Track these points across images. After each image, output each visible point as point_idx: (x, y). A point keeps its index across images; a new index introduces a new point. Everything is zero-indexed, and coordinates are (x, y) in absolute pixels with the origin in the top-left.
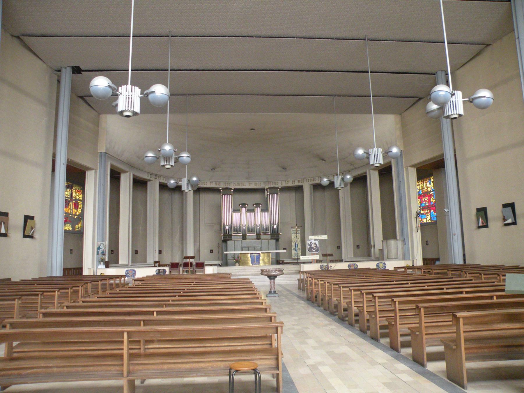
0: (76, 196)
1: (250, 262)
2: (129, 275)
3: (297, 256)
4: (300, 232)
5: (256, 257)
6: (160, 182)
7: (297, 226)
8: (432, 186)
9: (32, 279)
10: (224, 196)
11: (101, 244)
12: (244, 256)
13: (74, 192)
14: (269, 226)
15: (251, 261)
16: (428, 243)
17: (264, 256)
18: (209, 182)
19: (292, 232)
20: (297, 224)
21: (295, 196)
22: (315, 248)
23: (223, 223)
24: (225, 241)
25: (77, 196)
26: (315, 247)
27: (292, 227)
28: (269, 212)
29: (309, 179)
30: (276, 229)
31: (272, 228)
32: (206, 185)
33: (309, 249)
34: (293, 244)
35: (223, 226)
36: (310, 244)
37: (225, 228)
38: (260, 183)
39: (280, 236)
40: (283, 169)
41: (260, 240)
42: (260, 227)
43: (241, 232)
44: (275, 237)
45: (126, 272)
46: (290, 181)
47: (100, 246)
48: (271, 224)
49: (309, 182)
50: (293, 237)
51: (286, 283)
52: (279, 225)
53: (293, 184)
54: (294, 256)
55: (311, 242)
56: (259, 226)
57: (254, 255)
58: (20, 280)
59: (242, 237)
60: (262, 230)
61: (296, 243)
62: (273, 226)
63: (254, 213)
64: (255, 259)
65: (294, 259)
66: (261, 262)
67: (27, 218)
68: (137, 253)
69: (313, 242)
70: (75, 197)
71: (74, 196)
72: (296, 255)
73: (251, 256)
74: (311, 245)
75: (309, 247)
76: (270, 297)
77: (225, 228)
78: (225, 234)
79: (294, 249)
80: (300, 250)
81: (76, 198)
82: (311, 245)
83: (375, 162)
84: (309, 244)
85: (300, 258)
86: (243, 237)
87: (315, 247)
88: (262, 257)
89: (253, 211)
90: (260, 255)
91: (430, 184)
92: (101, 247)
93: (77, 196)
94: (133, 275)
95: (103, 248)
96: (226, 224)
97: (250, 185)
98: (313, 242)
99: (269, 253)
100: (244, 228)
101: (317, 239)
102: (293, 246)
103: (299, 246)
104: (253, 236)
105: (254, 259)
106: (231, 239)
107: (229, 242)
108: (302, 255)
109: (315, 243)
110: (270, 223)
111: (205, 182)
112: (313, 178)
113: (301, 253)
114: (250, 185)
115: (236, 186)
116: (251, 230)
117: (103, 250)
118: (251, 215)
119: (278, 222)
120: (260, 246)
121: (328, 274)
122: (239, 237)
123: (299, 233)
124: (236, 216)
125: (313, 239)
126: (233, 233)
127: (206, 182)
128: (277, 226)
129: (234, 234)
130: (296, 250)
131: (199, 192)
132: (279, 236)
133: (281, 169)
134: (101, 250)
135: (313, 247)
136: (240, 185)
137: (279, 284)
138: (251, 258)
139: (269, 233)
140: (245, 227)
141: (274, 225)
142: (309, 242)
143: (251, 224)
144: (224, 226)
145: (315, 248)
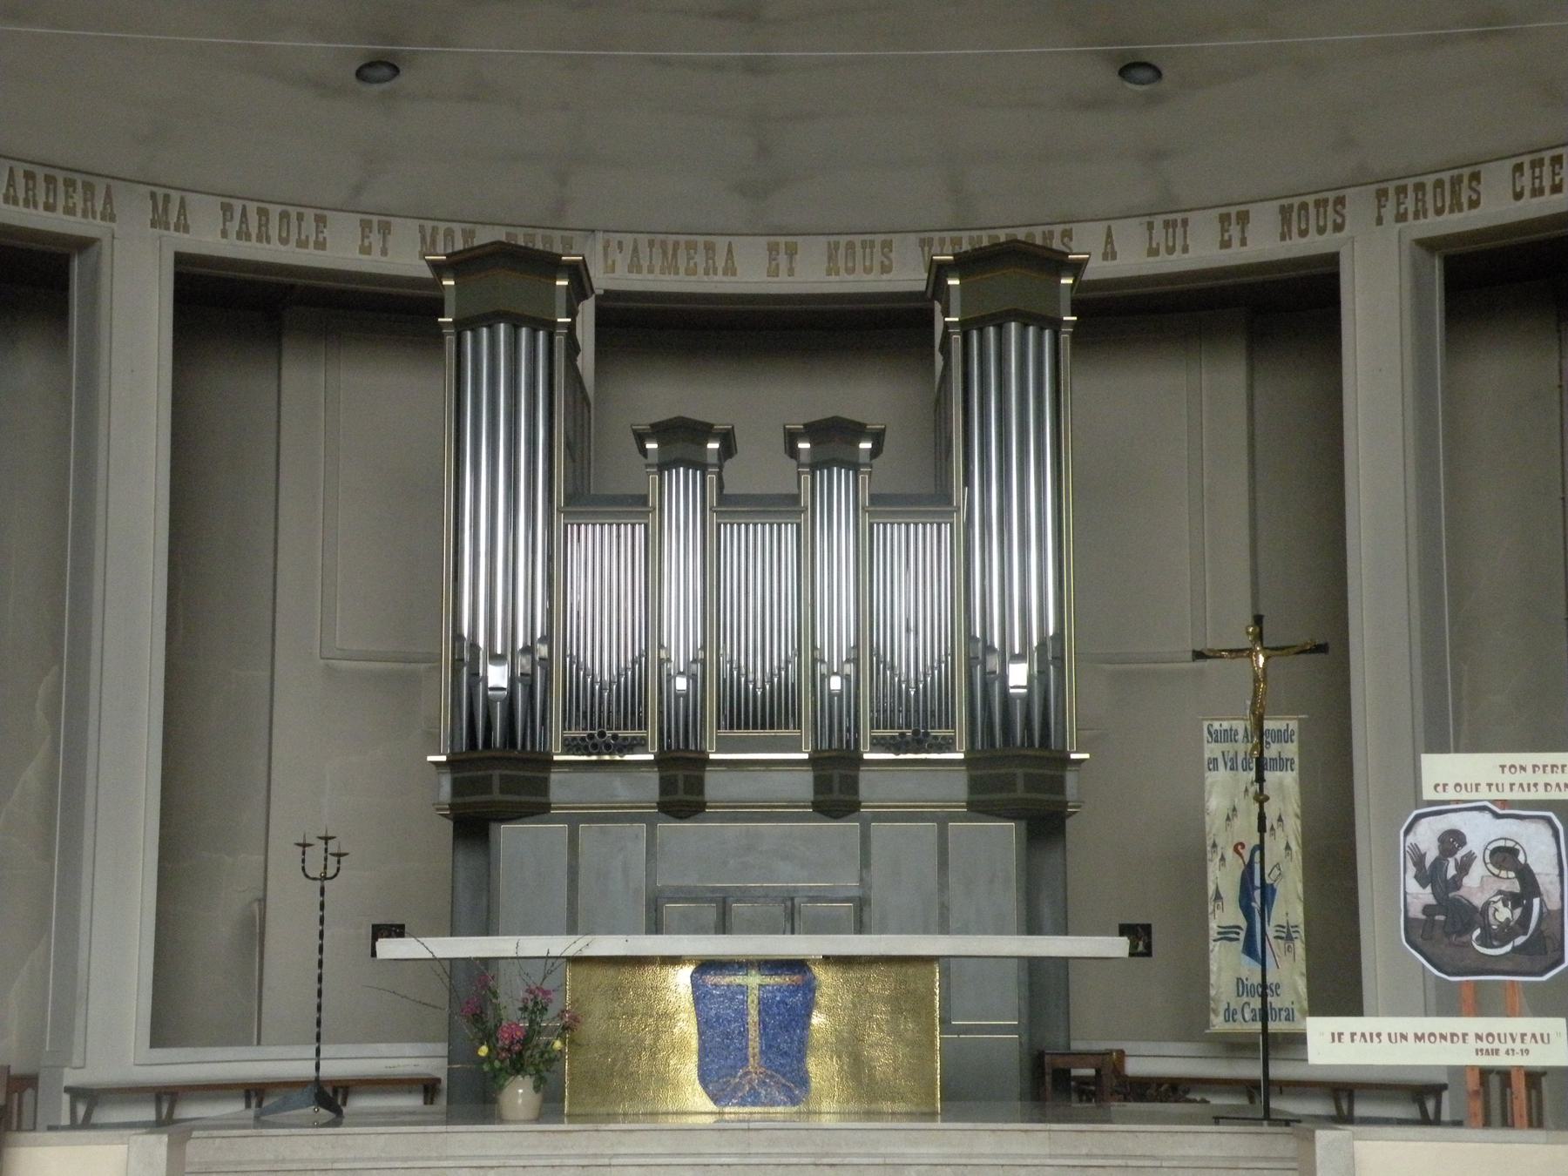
1: (687, 1068)
3: (1264, 1016)
4: (1291, 750)
5: (765, 1006)
7: (1259, 637)
12: (617, 991)
15: (703, 1052)
18: (356, 218)
19: (1212, 750)
20: (1258, 620)
21: (1251, 398)
22: (1504, 913)
23: (458, 636)
26: (1513, 899)
27: (1199, 655)
29: (1402, 190)
30: (1027, 700)
33: (1421, 932)
34: (1223, 877)
35: (457, 663)
36: (1439, 864)
38: (887, 245)
39: (1071, 778)
40: (1125, 72)
41: (851, 826)
42: (852, 683)
43: (651, 733)
44: (1020, 792)
46: (1193, 217)
49: (1401, 217)
50: (1216, 803)
52: (1059, 659)
53: (1226, 244)
54: (1230, 1015)
55: (1452, 840)
57: (743, 989)
59: (653, 779)
61: (1249, 867)
62: (994, 663)
63: (789, 532)
64: (753, 1032)
65: (1234, 1046)
66: (821, 1069)
69: (1481, 833)
72: (1256, 1003)
73: (700, 996)
74: (1451, 871)
75: (1420, 896)
79: (1227, 934)
80: (1299, 947)
82: (1451, 871)
83: (1284, 932)
84: (1432, 854)
85: (1299, 1039)
86: (666, 786)
87: (1513, 899)
88: (830, 1011)
89: (783, 506)
90: (809, 988)
96: (481, 643)
97: (783, 259)
98: (1481, 833)
99: (922, 970)
101: (1540, 795)
102: (1218, 897)
103: (1289, 907)
105: (743, 1034)
106: (539, 809)
107: (510, 836)
108: (1320, 1006)
109: (1504, 856)
111: (310, 214)
112: (1446, 176)
113: (1311, 976)
114: (783, 259)
115: (634, 267)
120: (850, 884)
122: (621, 789)
123: (1282, 763)
125: (1485, 795)
127: (321, 221)
128: (1043, 672)
130: (1249, 949)
131: (280, 345)
132: (1058, 785)
133: (1104, 78)
135: (1478, 901)
136: (682, 263)
138: (704, 1025)
139: (947, 745)
140: (692, 677)
141: (1007, 657)
142: (1426, 837)
144: (466, 661)
145: (1504, 913)
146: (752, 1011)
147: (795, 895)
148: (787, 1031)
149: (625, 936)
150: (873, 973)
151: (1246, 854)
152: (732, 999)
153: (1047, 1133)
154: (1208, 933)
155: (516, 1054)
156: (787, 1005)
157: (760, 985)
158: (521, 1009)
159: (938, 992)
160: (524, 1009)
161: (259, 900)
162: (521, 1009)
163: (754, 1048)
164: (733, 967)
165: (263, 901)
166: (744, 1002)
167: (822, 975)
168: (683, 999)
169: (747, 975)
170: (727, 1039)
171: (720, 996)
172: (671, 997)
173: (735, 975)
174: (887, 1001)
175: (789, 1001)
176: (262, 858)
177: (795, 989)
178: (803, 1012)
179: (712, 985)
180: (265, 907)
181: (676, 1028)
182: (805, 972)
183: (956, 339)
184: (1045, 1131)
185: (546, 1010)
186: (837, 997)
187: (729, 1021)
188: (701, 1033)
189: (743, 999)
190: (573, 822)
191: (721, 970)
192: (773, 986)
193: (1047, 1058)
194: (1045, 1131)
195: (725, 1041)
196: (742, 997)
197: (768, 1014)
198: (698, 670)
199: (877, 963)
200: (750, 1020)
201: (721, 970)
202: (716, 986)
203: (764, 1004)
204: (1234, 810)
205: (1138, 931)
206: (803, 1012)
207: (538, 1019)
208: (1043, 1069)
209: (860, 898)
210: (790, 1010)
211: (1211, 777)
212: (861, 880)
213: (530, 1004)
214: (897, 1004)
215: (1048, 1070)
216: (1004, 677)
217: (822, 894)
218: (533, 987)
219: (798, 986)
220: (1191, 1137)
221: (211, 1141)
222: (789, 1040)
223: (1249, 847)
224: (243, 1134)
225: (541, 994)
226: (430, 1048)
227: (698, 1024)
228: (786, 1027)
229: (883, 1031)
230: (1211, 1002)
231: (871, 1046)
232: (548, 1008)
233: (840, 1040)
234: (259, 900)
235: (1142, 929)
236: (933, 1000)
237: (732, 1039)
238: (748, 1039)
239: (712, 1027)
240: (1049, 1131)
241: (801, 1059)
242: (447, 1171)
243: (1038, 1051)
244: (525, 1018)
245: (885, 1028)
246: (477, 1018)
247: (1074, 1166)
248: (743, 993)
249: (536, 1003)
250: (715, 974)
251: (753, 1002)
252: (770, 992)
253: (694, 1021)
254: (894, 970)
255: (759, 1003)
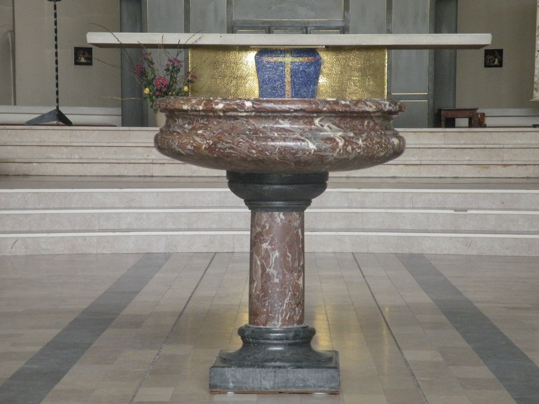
5: (294, 73)
12: (215, 65)
17: (345, 69)
45: (279, 129)
51: (469, 243)
57: (282, 64)
73: (260, 67)
76: (239, 391)
88: (328, 76)
90: (318, 64)
99: (379, 53)
137: (415, 250)
146: (287, 76)
147: (308, 26)
148: (306, 86)
149: (220, 34)
150: (352, 55)
152: (276, 70)
153: (443, 133)
154: (535, 47)
155: (163, 93)
156: (306, 72)
157: (292, 62)
158: (166, 70)
159: (386, 65)
160: (168, 70)
161: (11, 32)
162: (166, 70)
163: (288, 95)
164: (277, 52)
165: (13, 32)
166: (283, 71)
167: (325, 57)
168: (250, 69)
169: (284, 57)
170: (274, 90)
171: (270, 67)
172: (244, 68)
173: (278, 56)
174: (360, 70)
175: (306, 70)
176: (11, 8)
177: (309, 65)
178: (314, 76)
179: (266, 62)
180: (14, 36)
181: (247, 84)
182: (315, 55)
184: (442, 132)
185: (179, 71)
186: (332, 68)
187: (275, 81)
188: (260, 87)
189: (282, 70)
191: (271, 54)
192: (298, 63)
193: (443, 112)
194: (442, 132)
195: (273, 91)
196: (282, 68)
197: (296, 77)
199: (354, 50)
200: (286, 80)
201: (271, 54)
202: (268, 63)
203: (294, 72)
205: (495, 53)
206: (314, 76)
207: (175, 76)
208: (440, 118)
209: (343, 27)
210: (308, 75)
212: (344, 17)
213: (171, 68)
214: (363, 71)
215: (443, 118)
217: (323, 25)
218: (172, 59)
219: (312, 63)
220: (520, 134)
221: (5, 131)
222: (307, 91)
224: (22, 128)
225: (176, 63)
226: (110, 110)
227: (259, 82)
228: (305, 84)
229: (357, 86)
230: (535, 84)
231: (350, 93)
232: (180, 70)
233: (334, 91)
234: (11, 32)
235: (498, 52)
236: (384, 69)
237: (277, 90)
238: (285, 90)
239: (266, 84)
240: (445, 132)
242: (131, 148)
243: (437, 110)
244: (168, 75)
245: (358, 84)
246: (143, 73)
247: (457, 148)
248: (282, 66)
249: (174, 67)
250: (268, 56)
251: (288, 71)
252: (296, 66)
253: (256, 80)
254: (364, 54)
255: (291, 72)
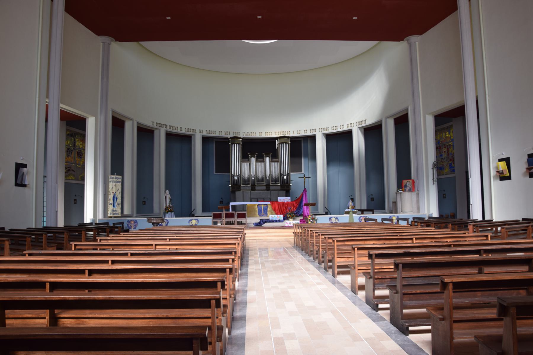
0: (79, 145)
2: (131, 225)
5: (264, 208)
6: (166, 131)
8: (451, 136)
9: (28, 228)
10: (232, 145)
11: (407, 181)
13: (77, 141)
14: (264, 177)
16: (445, 196)
24: (233, 192)
25: (80, 144)
28: (279, 162)
31: (282, 178)
32: (271, 135)
37: (233, 179)
42: (269, 178)
43: (250, 183)
47: (407, 184)
48: (281, 175)
56: (269, 177)
58: (9, 229)
60: (272, 180)
62: (283, 176)
63: (263, 163)
64: (263, 210)
67: (19, 166)
68: (145, 204)
70: (78, 146)
71: (77, 145)
73: (258, 207)
77: (233, 179)
78: (233, 184)
79: (111, 204)
81: (79, 147)
88: (269, 208)
91: (449, 134)
92: (407, 185)
93: (80, 144)
94: (135, 226)
95: (410, 186)
96: (234, 174)
100: (253, 178)
104: (263, 187)
105: (262, 210)
106: (240, 190)
110: (280, 174)
116: (260, 181)
117: (410, 187)
118: (260, 165)
119: (288, 173)
120: (269, 196)
121: (357, 227)
124: (245, 165)
126: (241, 183)
128: (287, 177)
129: (243, 184)
134: (408, 188)
138: (258, 209)
139: (249, 184)
141: (284, 175)
143: (260, 175)
151: (114, 193)
177: (266, 207)
183: (279, 145)
190: (271, 191)
198: (254, 177)
204: (113, 188)
210: (266, 208)
211: (110, 183)
216: (284, 177)
223: (114, 192)
228: (265, 210)
241: (267, 213)
